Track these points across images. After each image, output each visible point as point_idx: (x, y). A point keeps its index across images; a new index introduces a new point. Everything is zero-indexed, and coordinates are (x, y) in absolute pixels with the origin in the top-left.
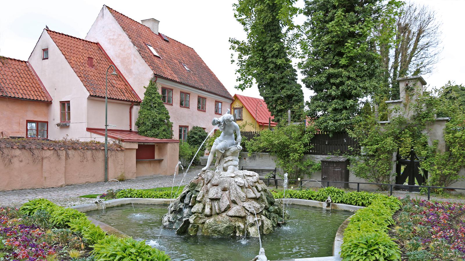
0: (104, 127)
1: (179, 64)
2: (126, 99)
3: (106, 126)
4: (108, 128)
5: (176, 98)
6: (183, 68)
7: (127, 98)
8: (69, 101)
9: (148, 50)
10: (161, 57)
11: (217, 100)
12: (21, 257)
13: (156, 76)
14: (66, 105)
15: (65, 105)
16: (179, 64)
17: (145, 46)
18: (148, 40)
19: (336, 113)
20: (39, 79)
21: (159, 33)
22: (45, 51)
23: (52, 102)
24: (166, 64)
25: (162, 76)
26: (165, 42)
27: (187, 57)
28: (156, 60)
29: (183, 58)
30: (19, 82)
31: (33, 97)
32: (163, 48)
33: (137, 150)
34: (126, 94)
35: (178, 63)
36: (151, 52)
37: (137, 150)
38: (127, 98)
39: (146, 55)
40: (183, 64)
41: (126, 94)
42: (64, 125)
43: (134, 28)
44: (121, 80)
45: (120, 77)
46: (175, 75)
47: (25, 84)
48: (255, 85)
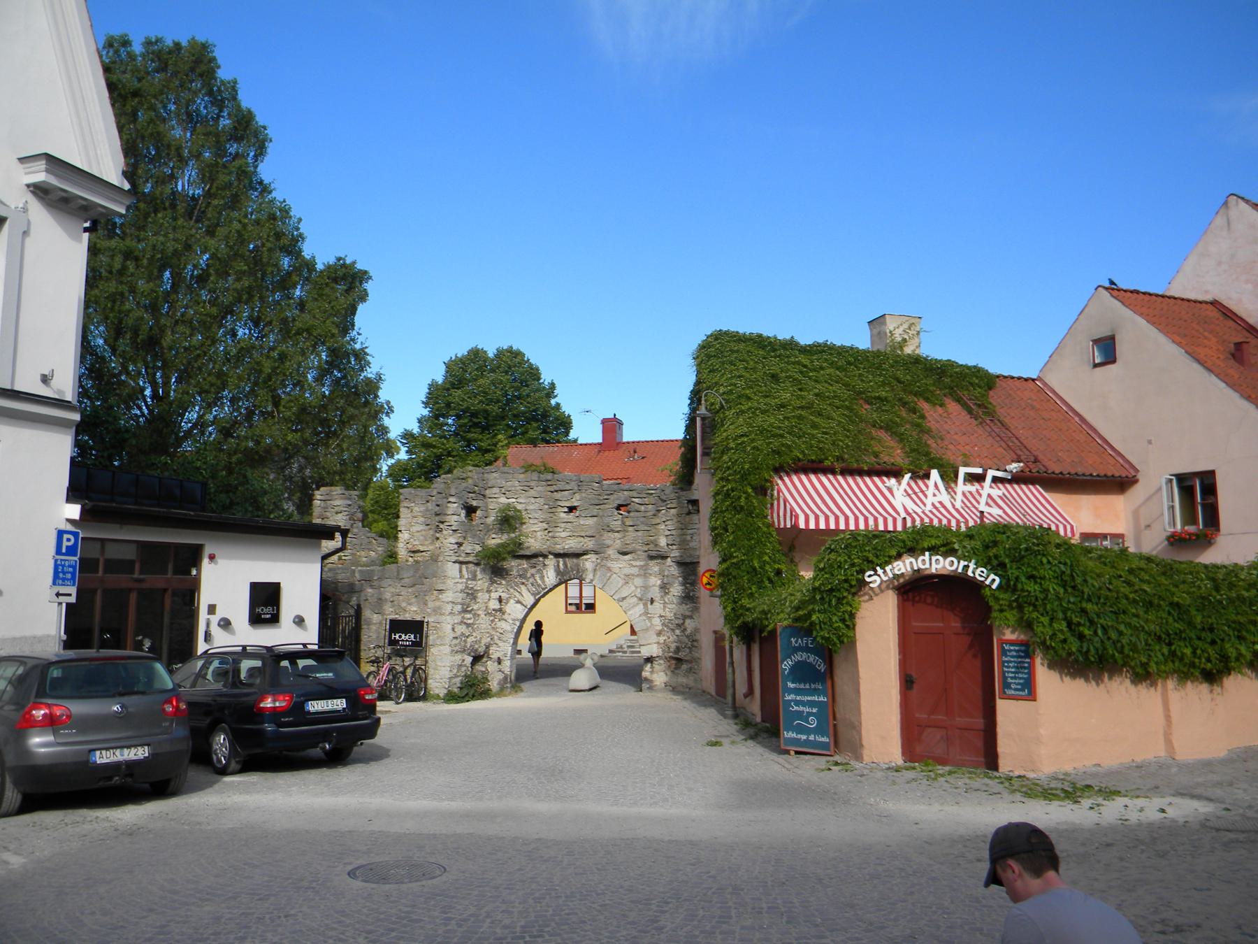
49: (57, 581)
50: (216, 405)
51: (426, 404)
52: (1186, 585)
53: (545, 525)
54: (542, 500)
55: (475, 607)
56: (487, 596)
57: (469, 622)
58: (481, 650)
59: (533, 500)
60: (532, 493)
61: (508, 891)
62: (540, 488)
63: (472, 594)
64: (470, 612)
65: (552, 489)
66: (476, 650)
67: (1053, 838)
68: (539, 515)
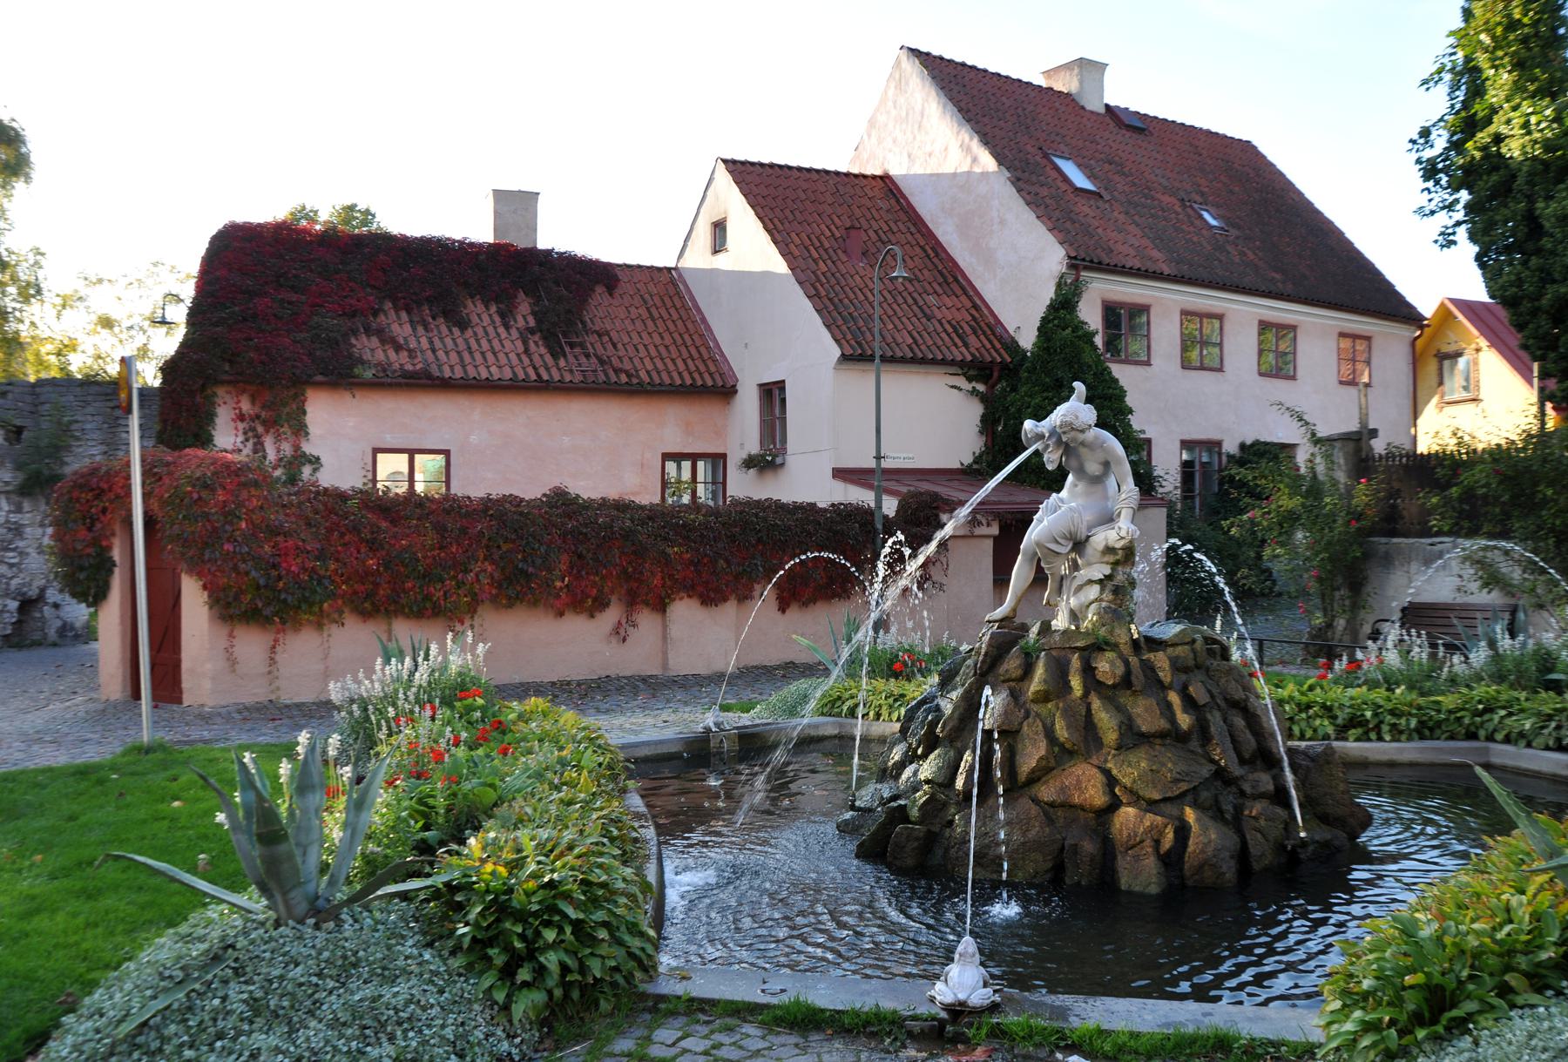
0: (872, 464)
1: (1179, 210)
2: (940, 357)
3: (878, 458)
4: (885, 464)
5: (1165, 333)
6: (1198, 223)
7: (972, 355)
8: (783, 381)
9: (1054, 174)
10: (1104, 193)
11: (1347, 331)
12: (207, 1018)
13: (1077, 263)
14: (776, 392)
15: (773, 394)
16: (1179, 210)
17: (1044, 161)
18: (1058, 139)
19: (895, 798)
20: (704, 320)
21: (1107, 106)
22: (719, 227)
23: (738, 387)
24: (1122, 217)
25: (1100, 263)
26: (1128, 134)
27: (1222, 178)
28: (1084, 208)
29: (1203, 182)
30: (644, 335)
31: (713, 379)
32: (1117, 159)
33: (996, 538)
34: (972, 340)
35: (1178, 203)
36: (1066, 179)
37: (996, 538)
38: (972, 355)
39: (1044, 192)
40: (1196, 206)
41: (972, 340)
42: (766, 462)
43: (1008, 103)
44: (959, 292)
45: (956, 280)
46: (1155, 254)
47: (662, 338)
48: (58, 376)
49: (1271, 336)
50: (20, 294)
51: (1243, 446)
52: (256, 852)
53: (104, 448)
54: (100, 418)
55: (21, 544)
56: (40, 531)
57: (12, 561)
58: (33, 593)
59: (90, 418)
60: (90, 410)
61: (140, 769)
62: (97, 404)
63: (16, 529)
64: (13, 550)
65: (112, 404)
66: (25, 594)
67: (925, 206)
68: (96, 435)
